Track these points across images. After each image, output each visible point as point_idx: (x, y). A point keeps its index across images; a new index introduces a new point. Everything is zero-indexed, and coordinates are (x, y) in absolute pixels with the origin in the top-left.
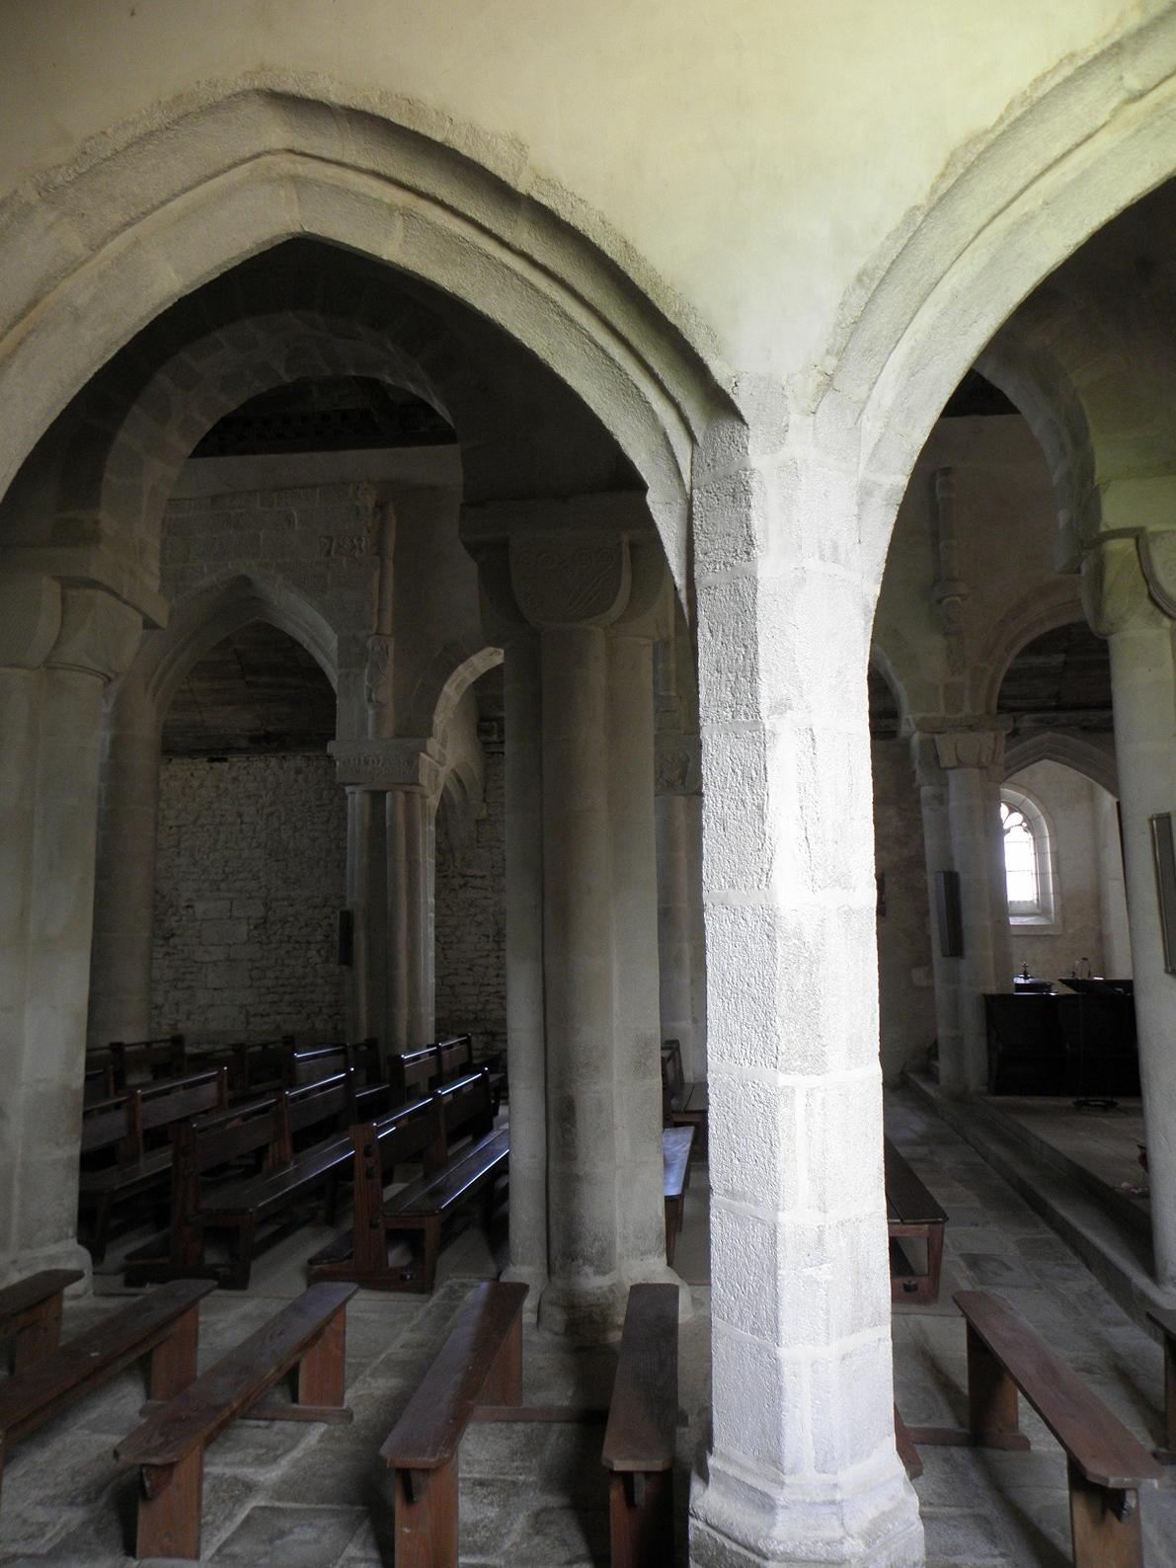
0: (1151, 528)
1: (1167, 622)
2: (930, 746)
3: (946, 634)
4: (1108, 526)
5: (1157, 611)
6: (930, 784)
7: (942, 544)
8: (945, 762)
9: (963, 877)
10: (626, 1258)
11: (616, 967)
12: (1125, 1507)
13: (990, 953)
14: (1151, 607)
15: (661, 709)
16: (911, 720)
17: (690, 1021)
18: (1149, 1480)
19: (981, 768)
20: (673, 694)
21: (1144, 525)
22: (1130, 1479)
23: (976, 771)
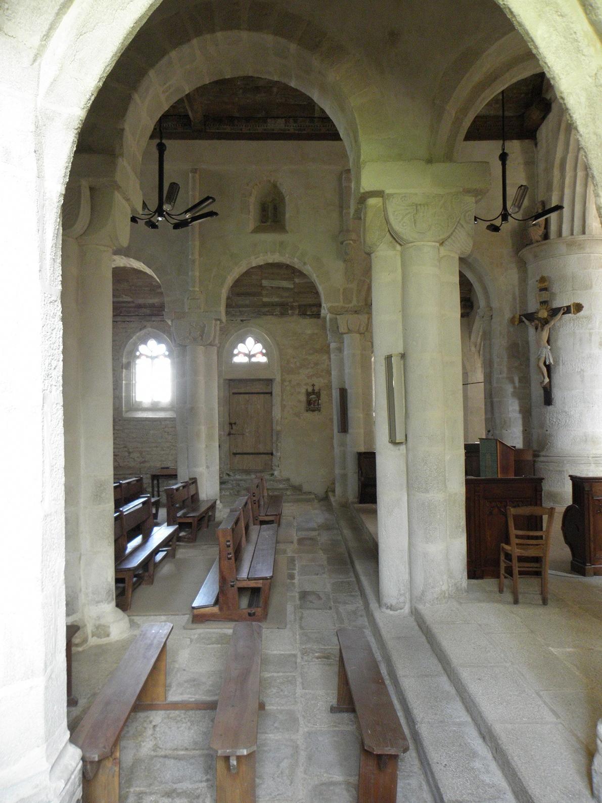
0: (387, 192)
1: (398, 247)
2: (334, 321)
3: (345, 261)
4: (364, 190)
5: (394, 241)
6: (335, 342)
7: (344, 211)
8: (342, 330)
9: (349, 391)
10: (87, 605)
11: (82, 441)
12: (231, 765)
13: (362, 431)
14: (391, 239)
15: (190, 298)
16: (325, 307)
17: (204, 468)
18: (241, 750)
19: (360, 334)
20: (197, 289)
21: (383, 189)
22: (231, 750)
23: (358, 335)
